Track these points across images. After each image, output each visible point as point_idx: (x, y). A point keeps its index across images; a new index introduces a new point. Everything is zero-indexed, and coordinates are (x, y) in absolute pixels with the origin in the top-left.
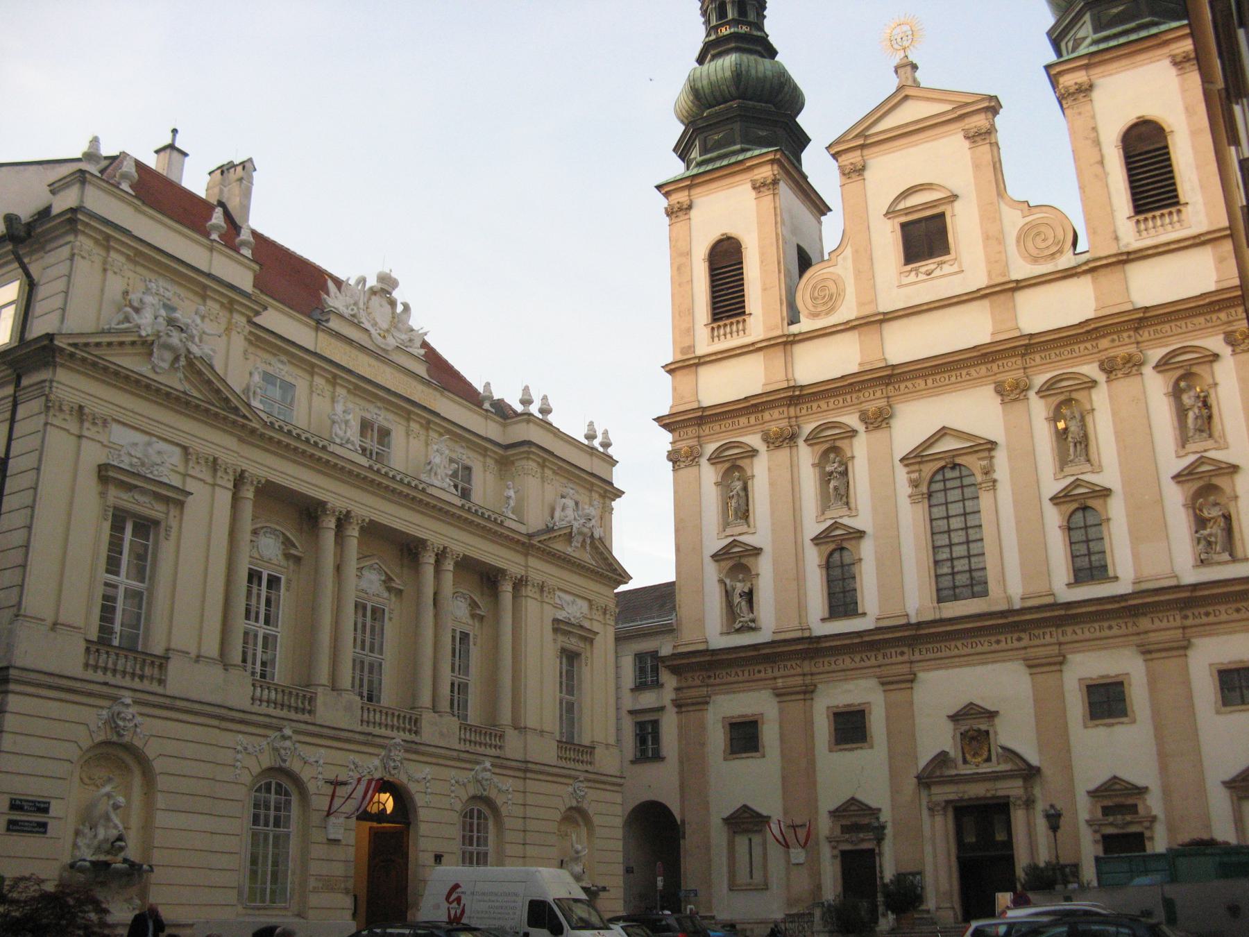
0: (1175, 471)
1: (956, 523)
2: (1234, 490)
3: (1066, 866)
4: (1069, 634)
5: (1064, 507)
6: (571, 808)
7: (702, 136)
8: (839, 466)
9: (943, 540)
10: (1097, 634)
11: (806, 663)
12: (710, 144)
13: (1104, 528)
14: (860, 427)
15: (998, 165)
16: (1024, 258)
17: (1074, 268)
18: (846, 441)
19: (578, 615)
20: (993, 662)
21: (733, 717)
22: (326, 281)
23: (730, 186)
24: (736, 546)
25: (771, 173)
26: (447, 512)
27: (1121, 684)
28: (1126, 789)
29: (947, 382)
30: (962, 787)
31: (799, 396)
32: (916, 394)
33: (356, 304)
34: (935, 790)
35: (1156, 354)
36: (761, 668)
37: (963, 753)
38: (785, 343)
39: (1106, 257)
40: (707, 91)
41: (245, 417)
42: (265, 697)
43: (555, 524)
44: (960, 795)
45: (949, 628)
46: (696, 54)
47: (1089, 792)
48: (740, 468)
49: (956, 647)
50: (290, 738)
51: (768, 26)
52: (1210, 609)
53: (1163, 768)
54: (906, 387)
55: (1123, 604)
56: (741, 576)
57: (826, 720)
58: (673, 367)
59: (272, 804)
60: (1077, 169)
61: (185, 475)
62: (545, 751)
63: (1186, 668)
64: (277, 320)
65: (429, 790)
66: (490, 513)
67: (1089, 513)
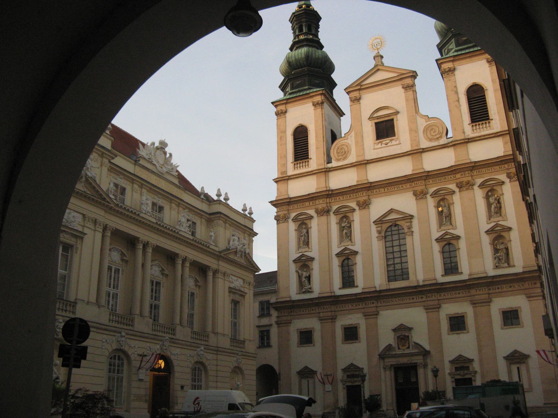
0: (486, 229)
1: (396, 249)
2: (510, 238)
3: (441, 392)
4: (443, 295)
5: (441, 243)
6: (236, 367)
7: (291, 82)
9: (391, 256)
10: (454, 296)
11: (333, 306)
12: (294, 85)
13: (457, 252)
14: (357, 208)
15: (416, 100)
16: (426, 139)
17: (447, 144)
19: (239, 285)
21: (301, 329)
22: (138, 143)
23: (303, 104)
24: (303, 257)
25: (320, 99)
26: (187, 242)
27: (463, 316)
28: (465, 360)
29: (335, 200)
31: (331, 194)
33: (150, 154)
34: (386, 360)
35: (479, 181)
37: (398, 345)
38: (325, 171)
39: (460, 140)
41: (108, 202)
42: (114, 319)
43: (230, 247)
44: (397, 362)
45: (392, 293)
46: (289, 46)
48: (306, 224)
50: (124, 336)
51: (320, 35)
52: (499, 286)
53: (480, 351)
54: (376, 191)
55: (464, 284)
56: (305, 270)
58: (278, 180)
59: (116, 365)
60: (448, 103)
61: (84, 226)
62: (225, 343)
63: (489, 311)
64: (121, 161)
65: (179, 359)
66: (204, 242)
67: (451, 246)
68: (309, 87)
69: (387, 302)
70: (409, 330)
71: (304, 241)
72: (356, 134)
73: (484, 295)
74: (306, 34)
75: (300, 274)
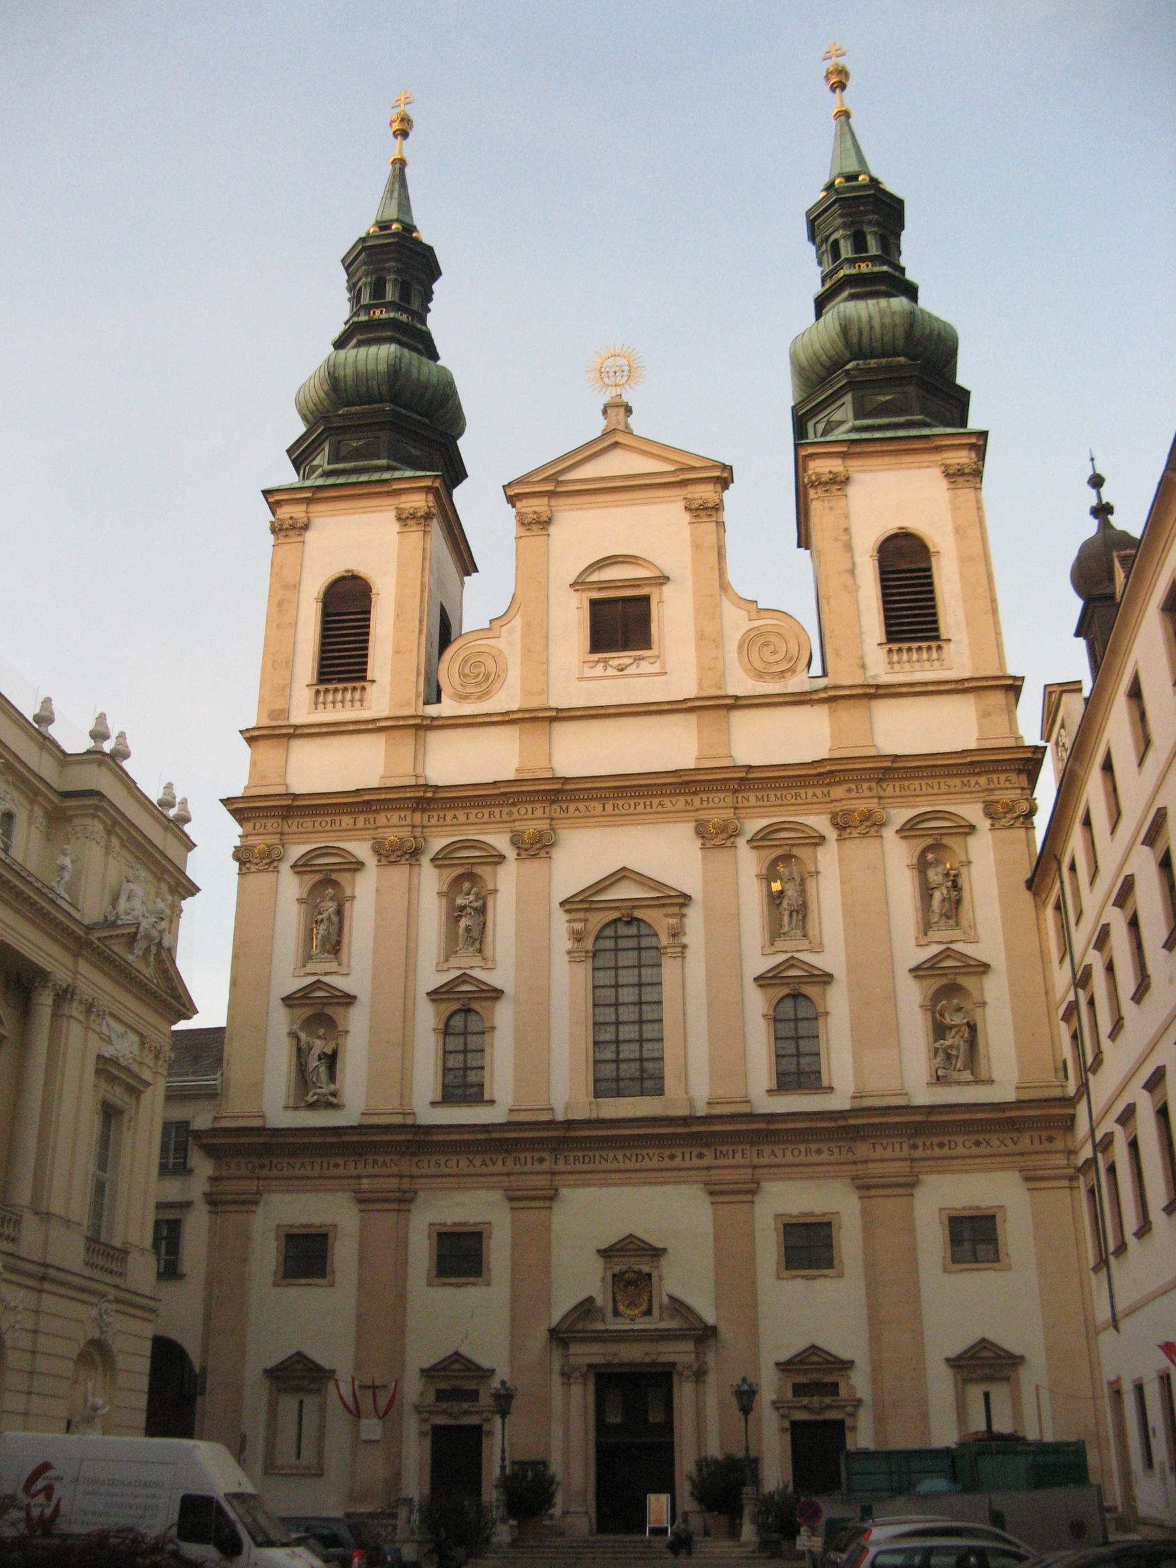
0: (913, 963)
4: (767, 1155)
7: (335, 439)
8: (476, 900)
9: (608, 1015)
10: (802, 1158)
12: (344, 451)
13: (821, 1021)
14: (510, 853)
16: (746, 671)
17: (810, 693)
21: (292, 1226)
25: (423, 504)
27: (829, 1224)
29: (632, 810)
30: (614, 1348)
31: (432, 799)
32: (587, 820)
34: (574, 1349)
38: (418, 727)
40: (349, 382)
43: (118, 917)
47: (778, 1364)
48: (335, 884)
49: (615, 1158)
52: (945, 1140)
53: (875, 1339)
54: (577, 809)
55: (841, 1123)
56: (321, 1031)
57: (427, 1242)
58: (256, 733)
63: (910, 1212)
71: (325, 940)
73: (899, 1164)
74: (852, 262)
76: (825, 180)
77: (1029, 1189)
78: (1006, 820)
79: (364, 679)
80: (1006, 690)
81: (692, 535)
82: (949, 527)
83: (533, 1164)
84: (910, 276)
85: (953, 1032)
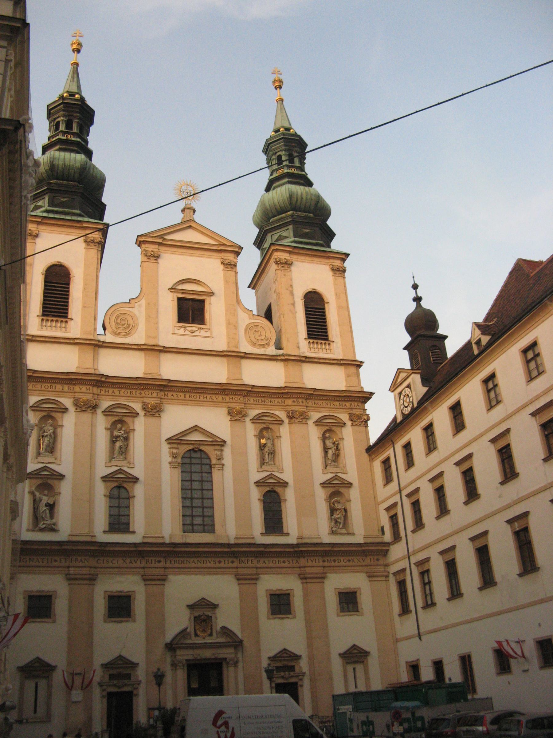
0: (322, 481)
4: (263, 562)
7: (53, 195)
8: (125, 433)
10: (277, 565)
16: (248, 342)
17: (277, 356)
18: (131, 419)
20: (50, 574)
21: (32, 591)
29: (205, 399)
30: (198, 652)
32: (177, 401)
34: (179, 652)
36: (58, 558)
37: (195, 630)
38: (95, 345)
39: (295, 356)
40: (60, 168)
48: (53, 418)
49: (194, 562)
52: (336, 558)
53: (310, 645)
55: (102, 548)
56: (46, 492)
68: (81, 213)
69: (180, 562)
70: (213, 608)
71: (48, 445)
72: (149, 304)
73: (319, 568)
74: (64, 133)
75: (38, 499)
76: (60, 92)
77: (370, 581)
78: (300, 419)
79: (66, 317)
80: (357, 367)
81: (224, 276)
82: (333, 293)
83: (155, 563)
84: (91, 146)
85: (338, 512)
